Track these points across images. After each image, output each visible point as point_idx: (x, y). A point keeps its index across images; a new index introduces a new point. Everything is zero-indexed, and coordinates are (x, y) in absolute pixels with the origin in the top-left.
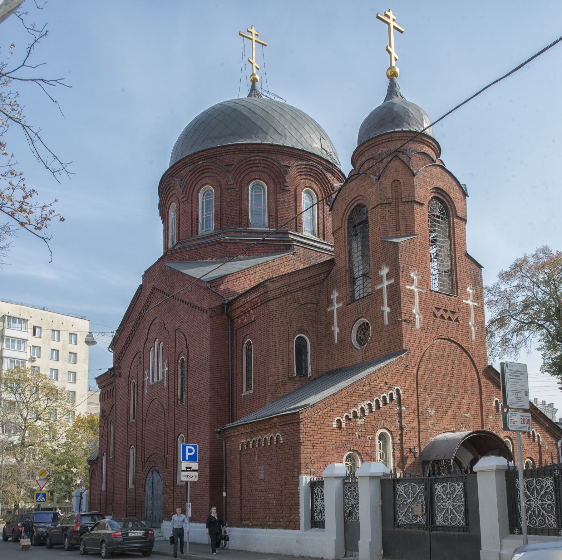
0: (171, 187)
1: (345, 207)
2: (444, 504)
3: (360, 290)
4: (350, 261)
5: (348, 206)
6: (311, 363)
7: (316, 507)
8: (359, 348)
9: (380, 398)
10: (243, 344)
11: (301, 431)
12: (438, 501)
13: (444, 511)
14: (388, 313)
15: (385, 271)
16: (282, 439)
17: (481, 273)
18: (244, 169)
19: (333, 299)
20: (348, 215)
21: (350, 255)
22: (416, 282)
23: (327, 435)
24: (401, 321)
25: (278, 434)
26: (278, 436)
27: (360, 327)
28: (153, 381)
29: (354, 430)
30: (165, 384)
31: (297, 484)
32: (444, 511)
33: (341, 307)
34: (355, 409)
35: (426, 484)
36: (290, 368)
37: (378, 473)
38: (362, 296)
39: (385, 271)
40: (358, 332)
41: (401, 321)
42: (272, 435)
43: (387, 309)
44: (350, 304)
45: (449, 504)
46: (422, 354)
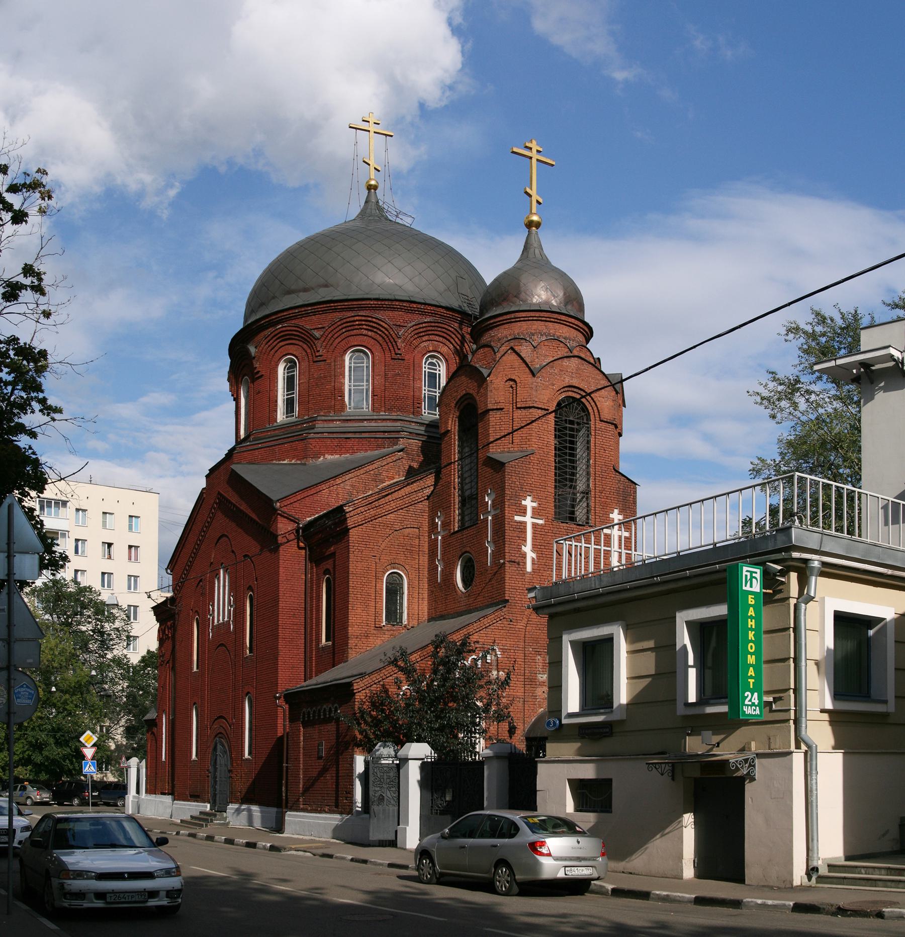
17: (635, 492)
18: (338, 334)
22: (529, 512)
24: (504, 563)
36: (377, 615)
41: (504, 563)
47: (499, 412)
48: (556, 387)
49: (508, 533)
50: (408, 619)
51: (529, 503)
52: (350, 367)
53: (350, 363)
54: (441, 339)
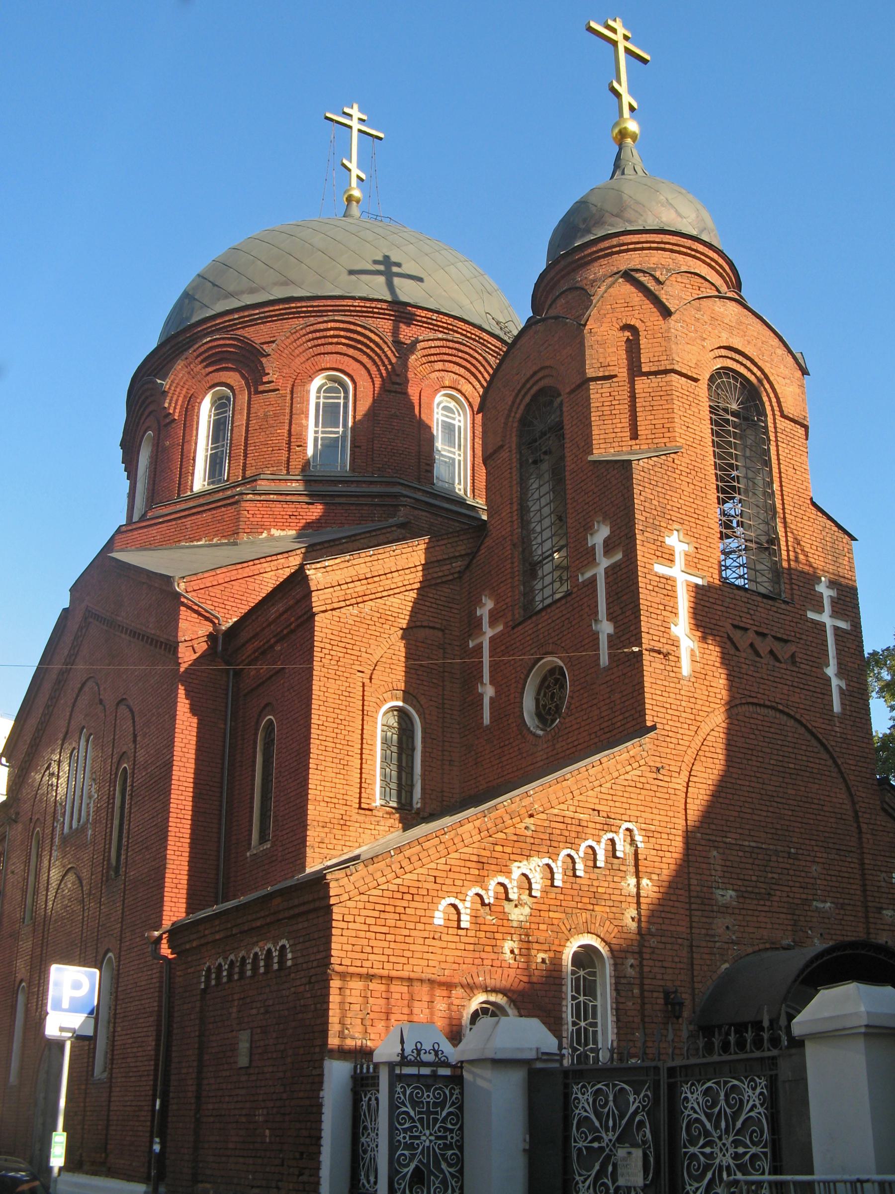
0: (147, 398)
1: (511, 398)
2: (708, 1150)
3: (549, 588)
4: (524, 523)
5: (517, 395)
6: (423, 776)
7: (365, 1152)
8: (541, 733)
9: (577, 851)
10: (257, 729)
11: (334, 931)
12: (693, 1142)
13: (709, 1175)
14: (609, 636)
15: (601, 534)
16: (289, 956)
19: (481, 617)
20: (518, 416)
21: (523, 510)
22: (679, 560)
23: (412, 947)
24: (641, 651)
25: (284, 942)
26: (283, 947)
27: (544, 680)
28: (71, 827)
29: (497, 936)
30: (90, 832)
31: (318, 1082)
32: (709, 1175)
33: (502, 634)
34: (502, 879)
35: (656, 1087)
37: (521, 1050)
38: (548, 601)
39: (601, 534)
40: (538, 694)
42: (269, 945)
43: (606, 628)
44: (520, 624)
45: (724, 1149)
46: (698, 740)
47: (606, 384)
48: (709, 345)
49: (643, 594)
50: (423, 798)
51: (675, 541)
52: (318, 405)
53: (318, 398)
54: (462, 371)
